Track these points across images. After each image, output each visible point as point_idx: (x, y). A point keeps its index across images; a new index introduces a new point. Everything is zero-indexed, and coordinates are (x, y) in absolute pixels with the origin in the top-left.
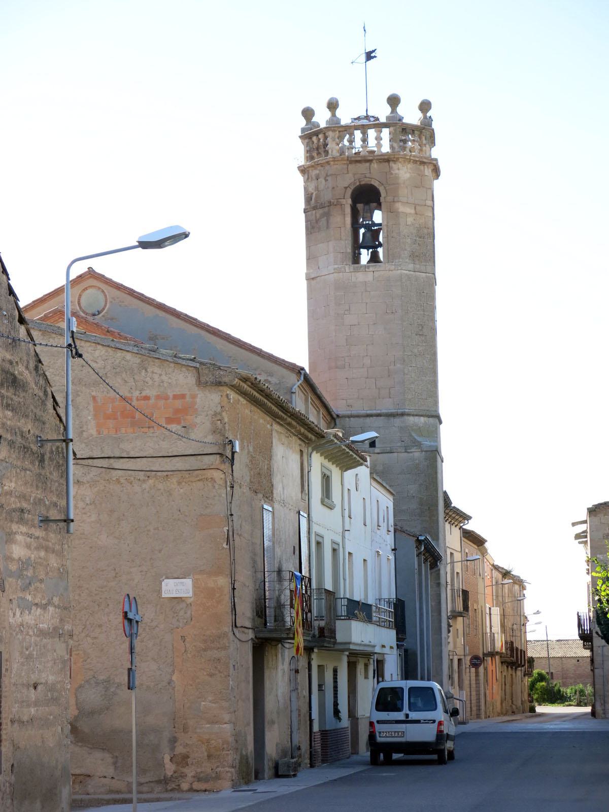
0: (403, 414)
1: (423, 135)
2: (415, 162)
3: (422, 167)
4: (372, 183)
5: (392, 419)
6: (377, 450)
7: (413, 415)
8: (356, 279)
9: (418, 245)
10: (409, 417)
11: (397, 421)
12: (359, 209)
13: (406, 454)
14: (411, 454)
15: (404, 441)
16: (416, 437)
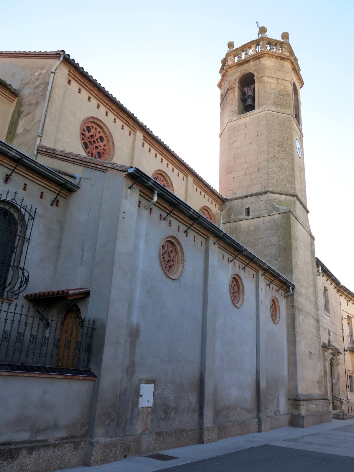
0: (267, 192)
1: (284, 48)
2: (277, 57)
3: (282, 62)
4: (250, 72)
5: (260, 197)
6: (250, 217)
7: (275, 193)
8: (240, 122)
9: (279, 99)
10: (272, 194)
11: (264, 197)
12: (245, 90)
13: (269, 217)
14: (273, 217)
15: (267, 209)
16: (276, 206)
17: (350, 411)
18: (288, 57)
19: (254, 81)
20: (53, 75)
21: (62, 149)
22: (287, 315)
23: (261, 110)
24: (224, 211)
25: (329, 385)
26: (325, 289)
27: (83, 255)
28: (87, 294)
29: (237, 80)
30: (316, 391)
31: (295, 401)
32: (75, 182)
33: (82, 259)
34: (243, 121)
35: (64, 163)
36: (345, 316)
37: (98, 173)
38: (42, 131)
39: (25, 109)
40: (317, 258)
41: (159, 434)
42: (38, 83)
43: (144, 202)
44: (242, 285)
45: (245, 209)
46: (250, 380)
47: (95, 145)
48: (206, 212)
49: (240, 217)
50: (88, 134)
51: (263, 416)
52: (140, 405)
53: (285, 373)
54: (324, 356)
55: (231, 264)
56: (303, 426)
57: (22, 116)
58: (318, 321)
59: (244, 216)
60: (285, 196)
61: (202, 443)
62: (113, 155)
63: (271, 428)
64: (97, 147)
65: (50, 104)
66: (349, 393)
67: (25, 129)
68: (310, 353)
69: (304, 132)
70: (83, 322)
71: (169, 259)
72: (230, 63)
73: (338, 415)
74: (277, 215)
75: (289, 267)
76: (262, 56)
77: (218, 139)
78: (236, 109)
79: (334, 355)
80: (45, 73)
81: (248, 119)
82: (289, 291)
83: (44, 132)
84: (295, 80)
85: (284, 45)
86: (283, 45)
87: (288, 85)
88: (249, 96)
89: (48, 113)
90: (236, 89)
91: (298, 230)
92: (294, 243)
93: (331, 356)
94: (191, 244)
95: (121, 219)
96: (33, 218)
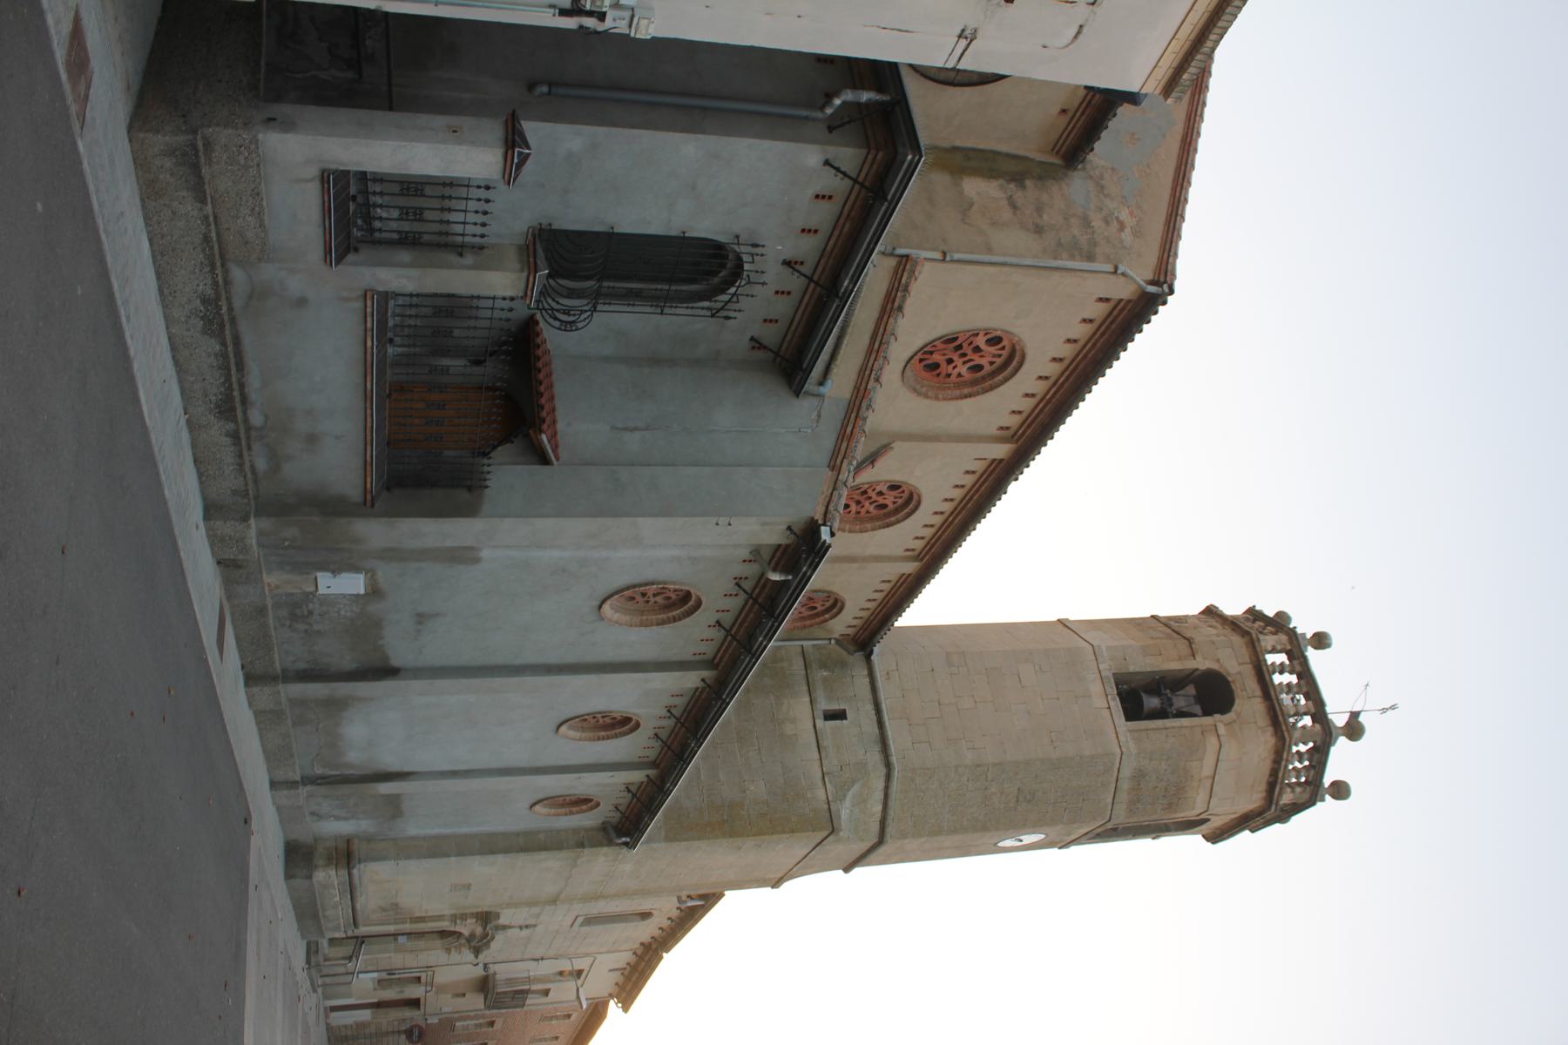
5: (877, 748)
6: (820, 723)
11: (875, 757)
14: (820, 783)
17: (328, 980)
19: (1206, 721)
20: (1110, 268)
21: (899, 332)
22: (558, 831)
23: (1122, 739)
24: (838, 648)
25: (391, 928)
26: (645, 915)
27: (636, 429)
28: (544, 460)
29: (1215, 666)
30: (369, 900)
31: (346, 855)
32: (810, 385)
33: (626, 429)
34: (1096, 688)
35: (866, 340)
36: (579, 964)
37: (828, 443)
38: (959, 261)
39: (1029, 195)
40: (721, 895)
41: (262, 611)
42: (1097, 223)
43: (766, 555)
44: (616, 736)
45: (842, 707)
46: (390, 762)
47: (955, 358)
48: (828, 604)
49: (820, 695)
50: (981, 341)
51: (304, 791)
52: (319, 574)
53: (412, 831)
54: (464, 917)
55: (664, 712)
56: (289, 876)
57: (1012, 186)
58: (554, 901)
59: (824, 705)
61: (247, 684)
62: (937, 398)
63: (279, 809)
64: (950, 361)
65: (1033, 271)
66: (375, 975)
67: (971, 205)
68: (469, 887)
69: (1074, 849)
70: (485, 455)
71: (650, 594)
72: (1268, 640)
73: (317, 952)
74: (824, 797)
75: (683, 831)
77: (1052, 617)
78: (1132, 669)
79: (468, 941)
80: (1122, 241)
81: (1100, 702)
82: (620, 835)
83: (955, 266)
84: (1216, 822)
88: (1169, 700)
89: (1006, 269)
90: (1191, 664)
91: (797, 847)
92: (750, 842)
93: (466, 932)
94: (695, 635)
95: (714, 520)
96: (713, 316)
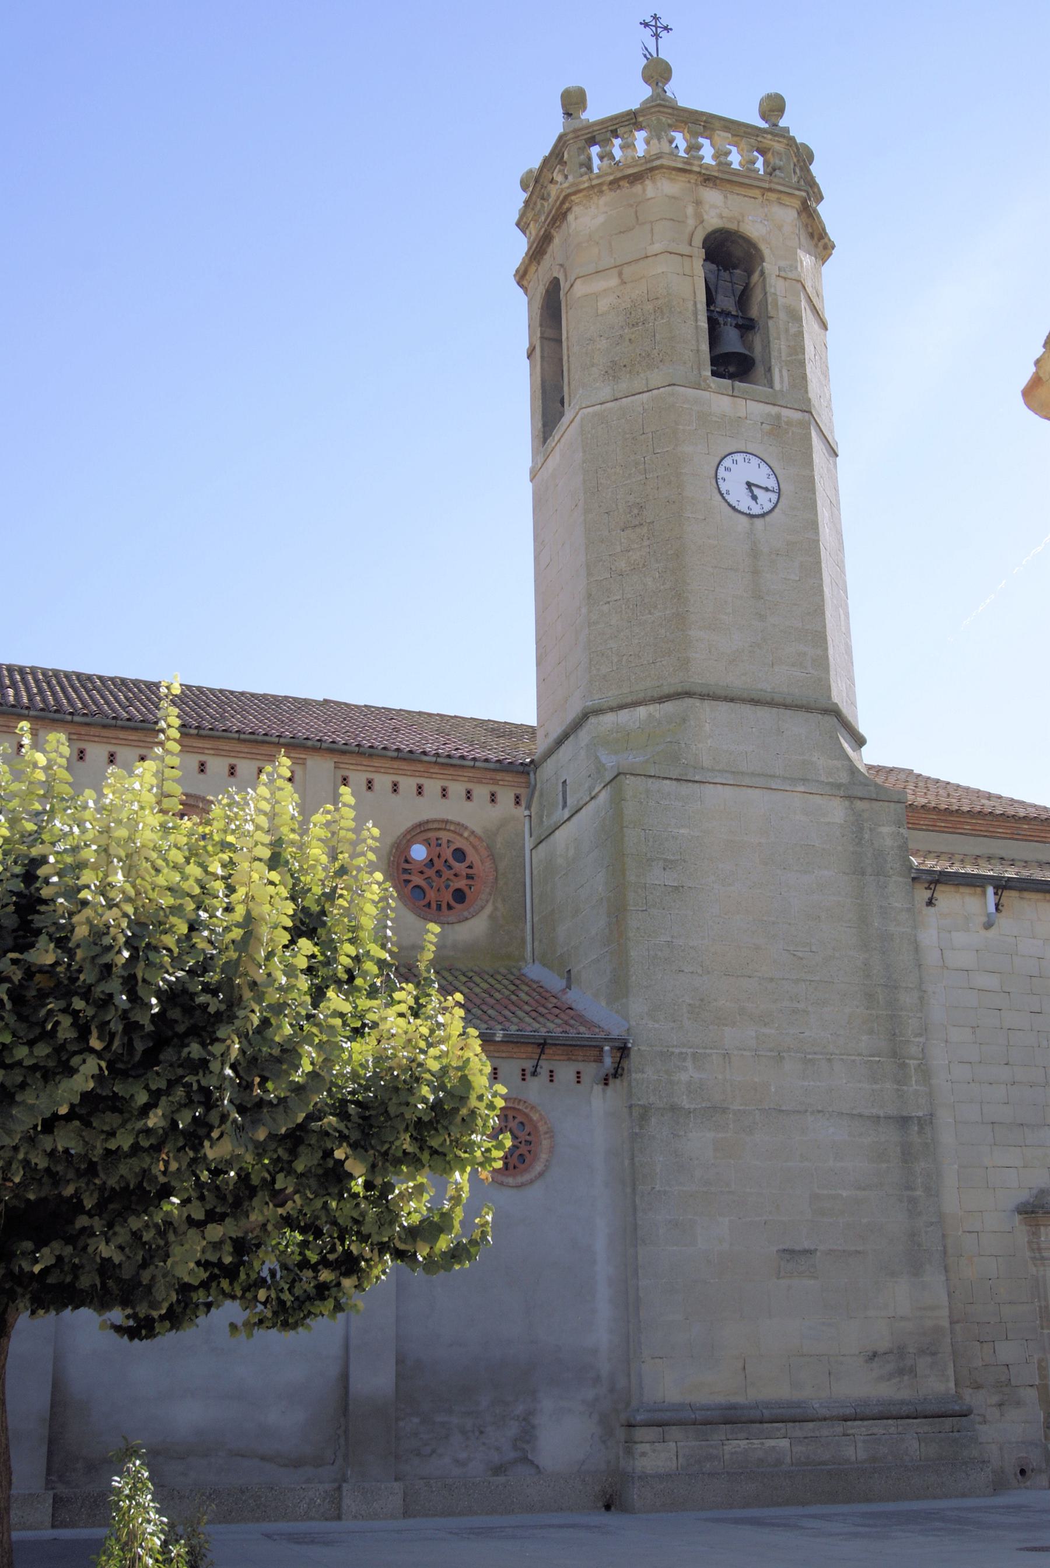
3: (638, 188)
7: (612, 709)
18: (649, 166)
60: (647, 707)
76: (566, 205)
85: (644, 116)
86: (641, 119)
87: (660, 271)
